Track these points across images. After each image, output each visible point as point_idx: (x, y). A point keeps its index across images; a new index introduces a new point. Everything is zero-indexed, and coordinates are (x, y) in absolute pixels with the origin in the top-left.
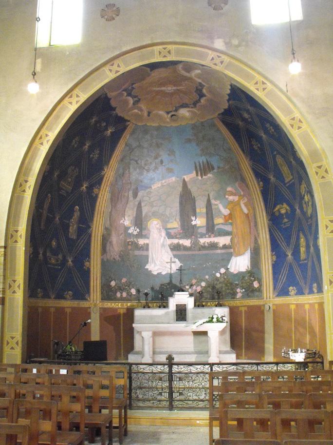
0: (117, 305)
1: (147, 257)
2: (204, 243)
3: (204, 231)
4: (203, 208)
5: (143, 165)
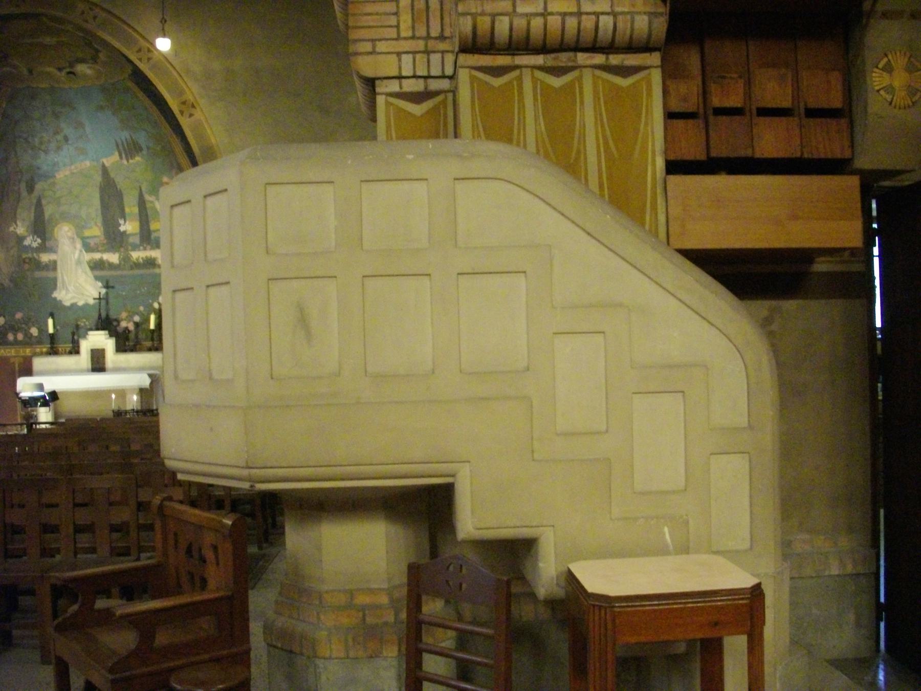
0: (9, 352)
1: (54, 281)
2: (137, 259)
3: (136, 240)
4: (134, 206)
5: (37, 145)
